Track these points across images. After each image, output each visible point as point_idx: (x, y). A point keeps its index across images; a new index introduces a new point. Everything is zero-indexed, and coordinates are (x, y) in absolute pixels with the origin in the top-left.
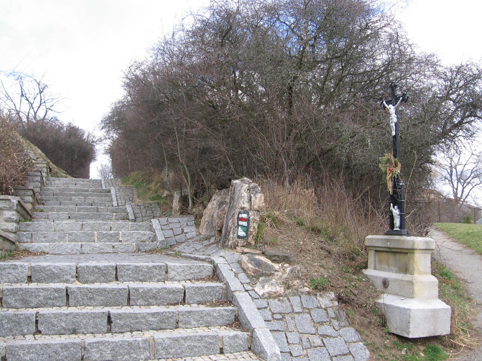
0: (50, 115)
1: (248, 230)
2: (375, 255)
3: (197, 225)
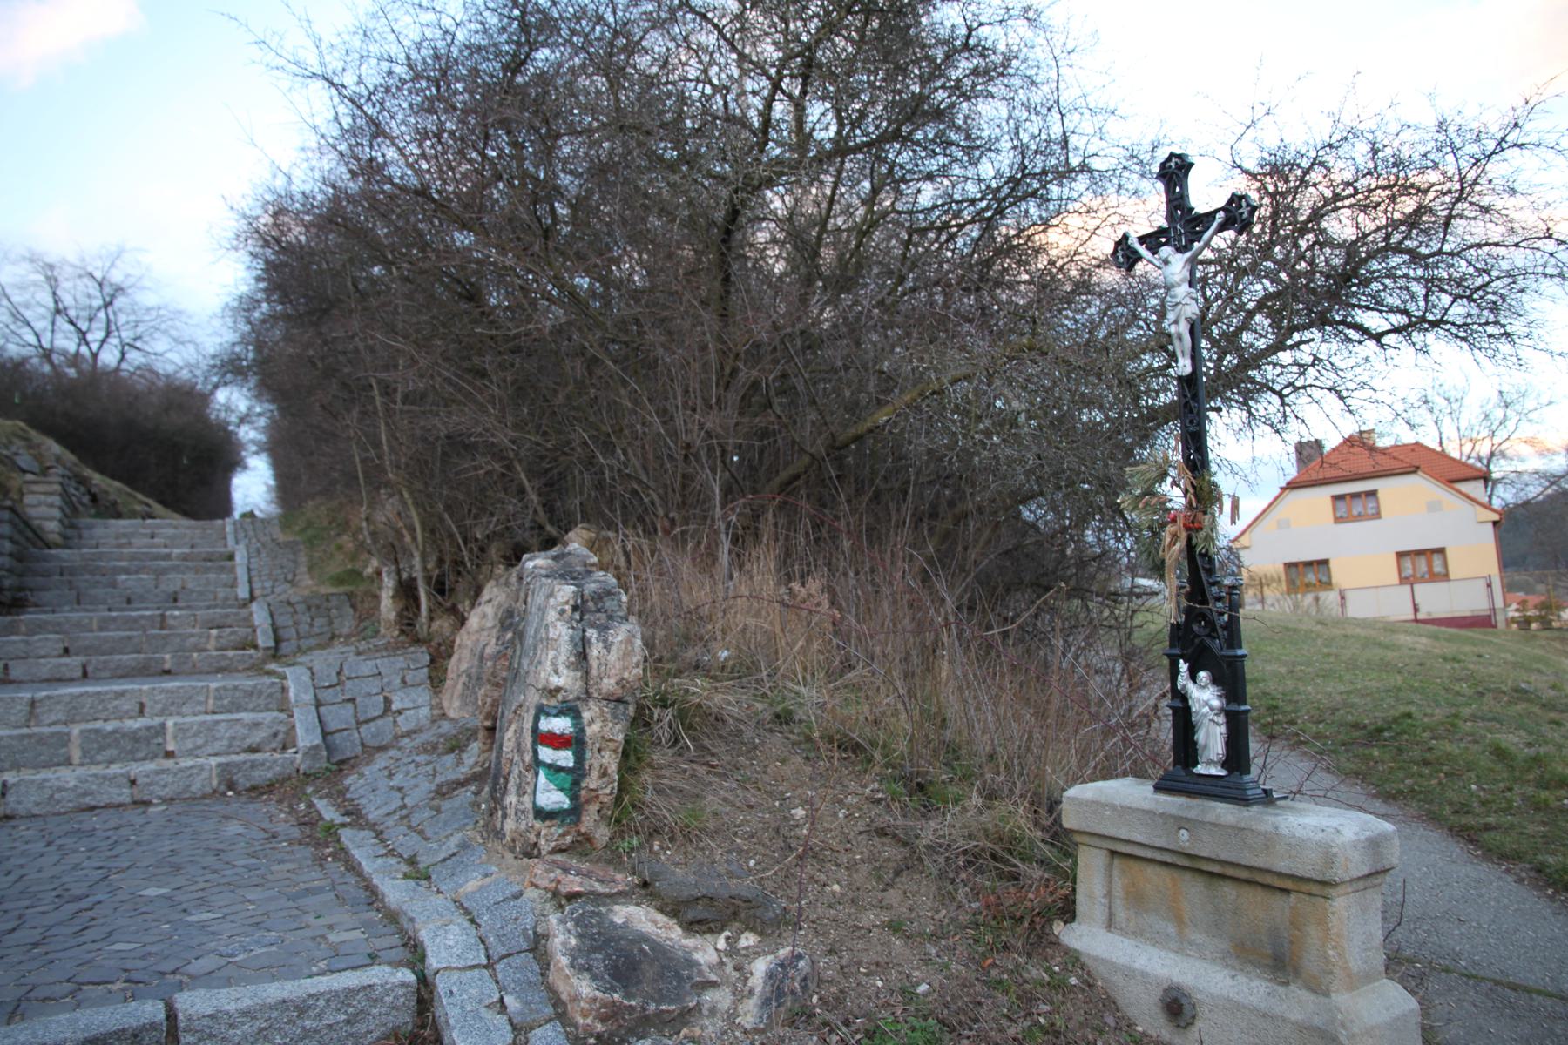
0: (134, 357)
1: (576, 783)
2: (1110, 867)
3: (436, 679)
